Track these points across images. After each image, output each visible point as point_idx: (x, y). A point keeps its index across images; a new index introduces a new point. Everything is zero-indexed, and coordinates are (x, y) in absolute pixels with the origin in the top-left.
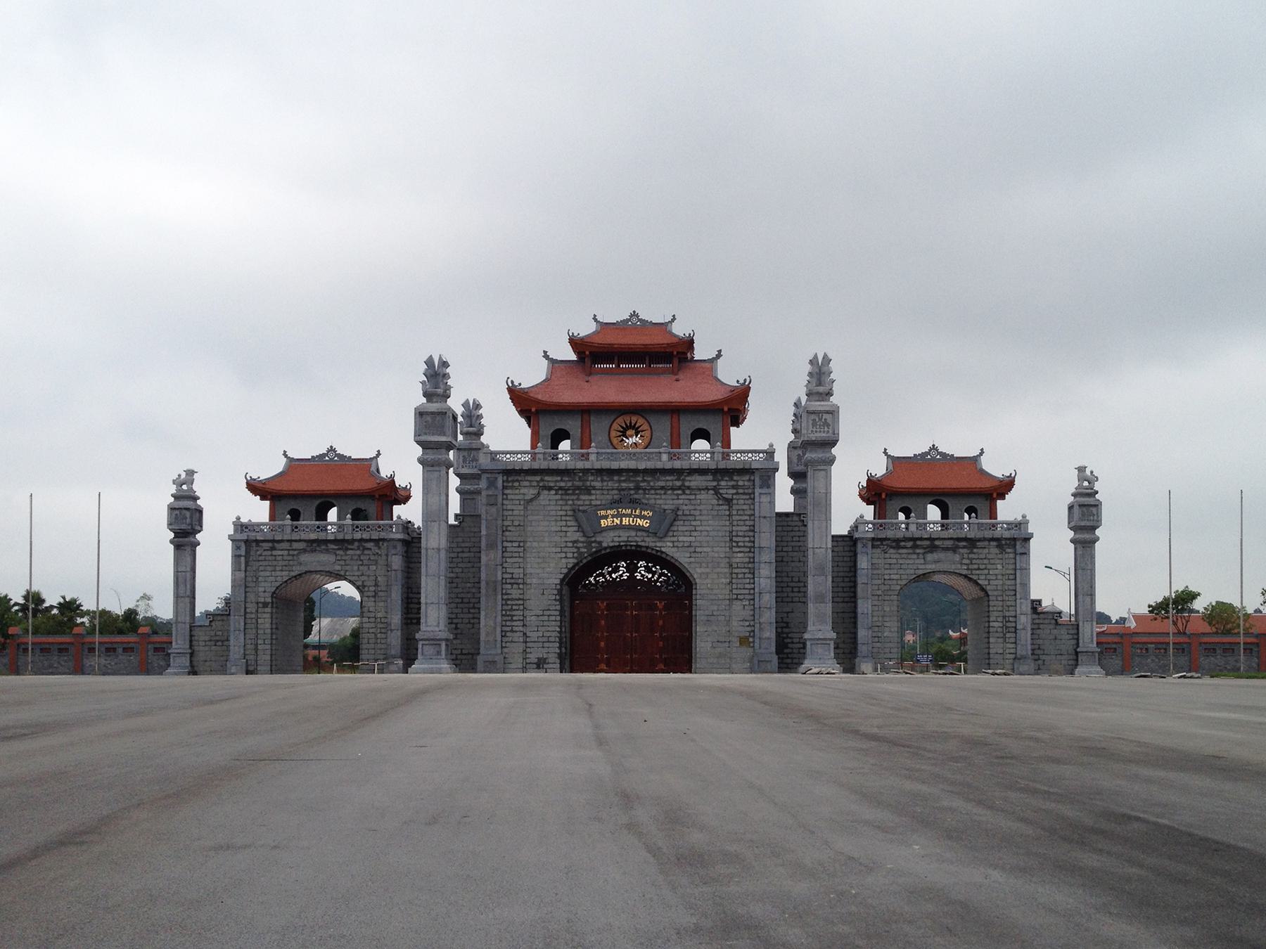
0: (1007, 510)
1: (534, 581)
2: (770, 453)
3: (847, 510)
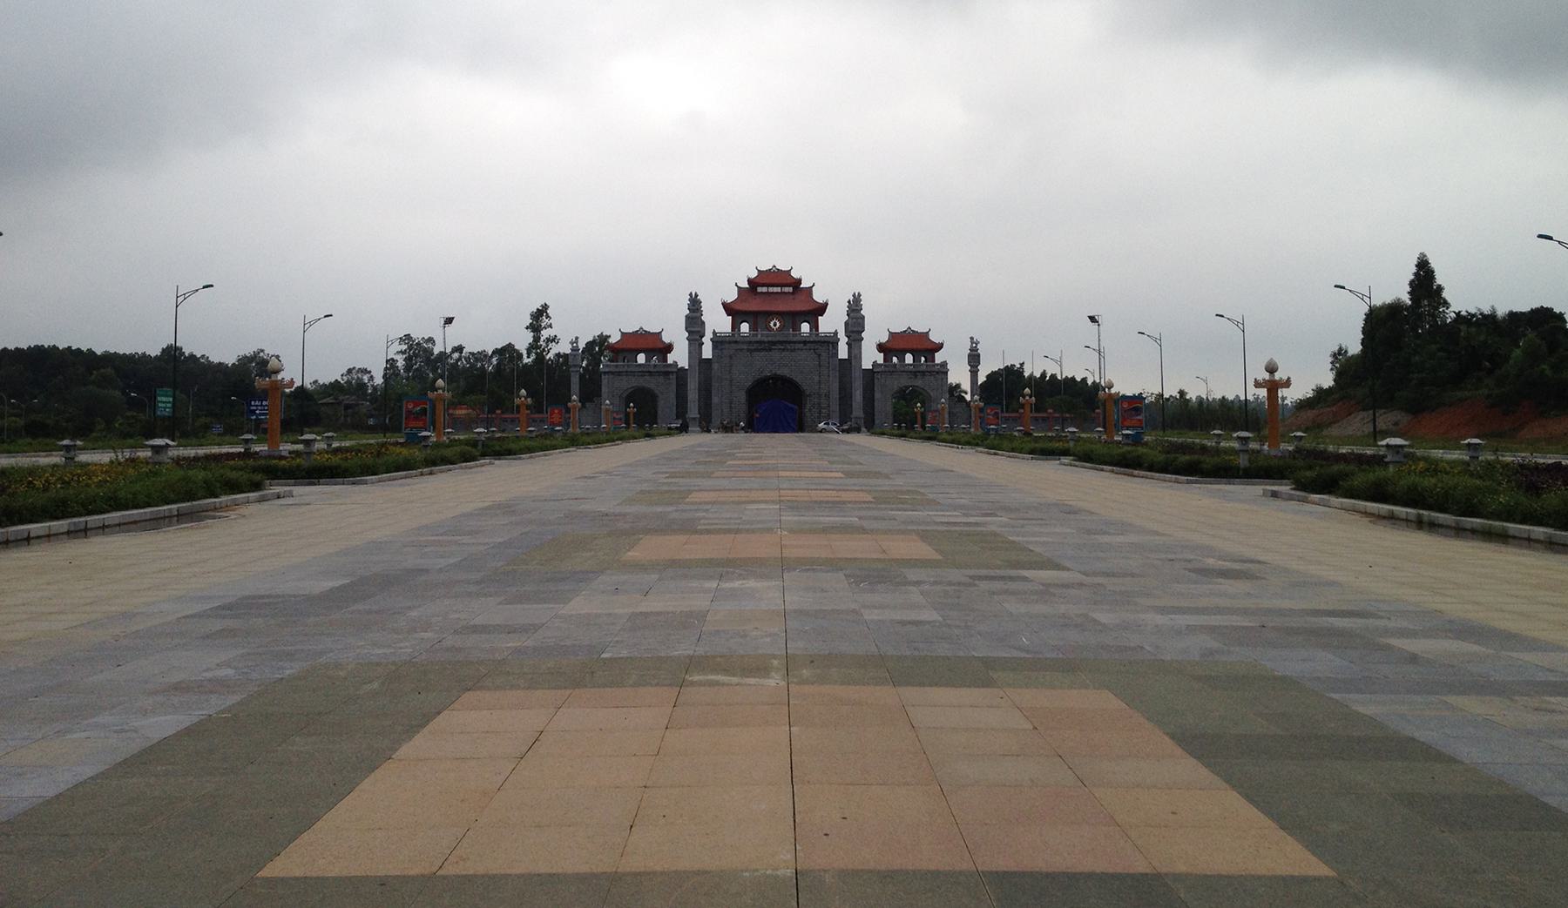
0: (939, 357)
1: (805, 673)
2: (836, 333)
3: (870, 357)
